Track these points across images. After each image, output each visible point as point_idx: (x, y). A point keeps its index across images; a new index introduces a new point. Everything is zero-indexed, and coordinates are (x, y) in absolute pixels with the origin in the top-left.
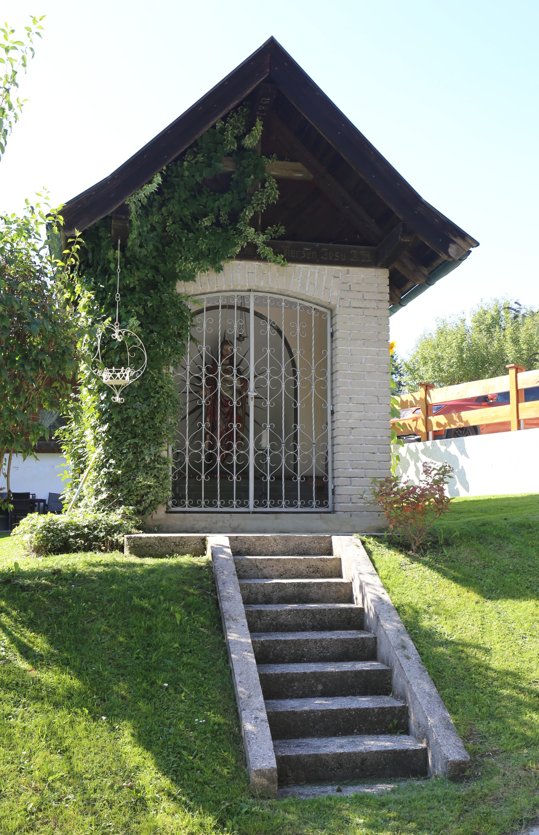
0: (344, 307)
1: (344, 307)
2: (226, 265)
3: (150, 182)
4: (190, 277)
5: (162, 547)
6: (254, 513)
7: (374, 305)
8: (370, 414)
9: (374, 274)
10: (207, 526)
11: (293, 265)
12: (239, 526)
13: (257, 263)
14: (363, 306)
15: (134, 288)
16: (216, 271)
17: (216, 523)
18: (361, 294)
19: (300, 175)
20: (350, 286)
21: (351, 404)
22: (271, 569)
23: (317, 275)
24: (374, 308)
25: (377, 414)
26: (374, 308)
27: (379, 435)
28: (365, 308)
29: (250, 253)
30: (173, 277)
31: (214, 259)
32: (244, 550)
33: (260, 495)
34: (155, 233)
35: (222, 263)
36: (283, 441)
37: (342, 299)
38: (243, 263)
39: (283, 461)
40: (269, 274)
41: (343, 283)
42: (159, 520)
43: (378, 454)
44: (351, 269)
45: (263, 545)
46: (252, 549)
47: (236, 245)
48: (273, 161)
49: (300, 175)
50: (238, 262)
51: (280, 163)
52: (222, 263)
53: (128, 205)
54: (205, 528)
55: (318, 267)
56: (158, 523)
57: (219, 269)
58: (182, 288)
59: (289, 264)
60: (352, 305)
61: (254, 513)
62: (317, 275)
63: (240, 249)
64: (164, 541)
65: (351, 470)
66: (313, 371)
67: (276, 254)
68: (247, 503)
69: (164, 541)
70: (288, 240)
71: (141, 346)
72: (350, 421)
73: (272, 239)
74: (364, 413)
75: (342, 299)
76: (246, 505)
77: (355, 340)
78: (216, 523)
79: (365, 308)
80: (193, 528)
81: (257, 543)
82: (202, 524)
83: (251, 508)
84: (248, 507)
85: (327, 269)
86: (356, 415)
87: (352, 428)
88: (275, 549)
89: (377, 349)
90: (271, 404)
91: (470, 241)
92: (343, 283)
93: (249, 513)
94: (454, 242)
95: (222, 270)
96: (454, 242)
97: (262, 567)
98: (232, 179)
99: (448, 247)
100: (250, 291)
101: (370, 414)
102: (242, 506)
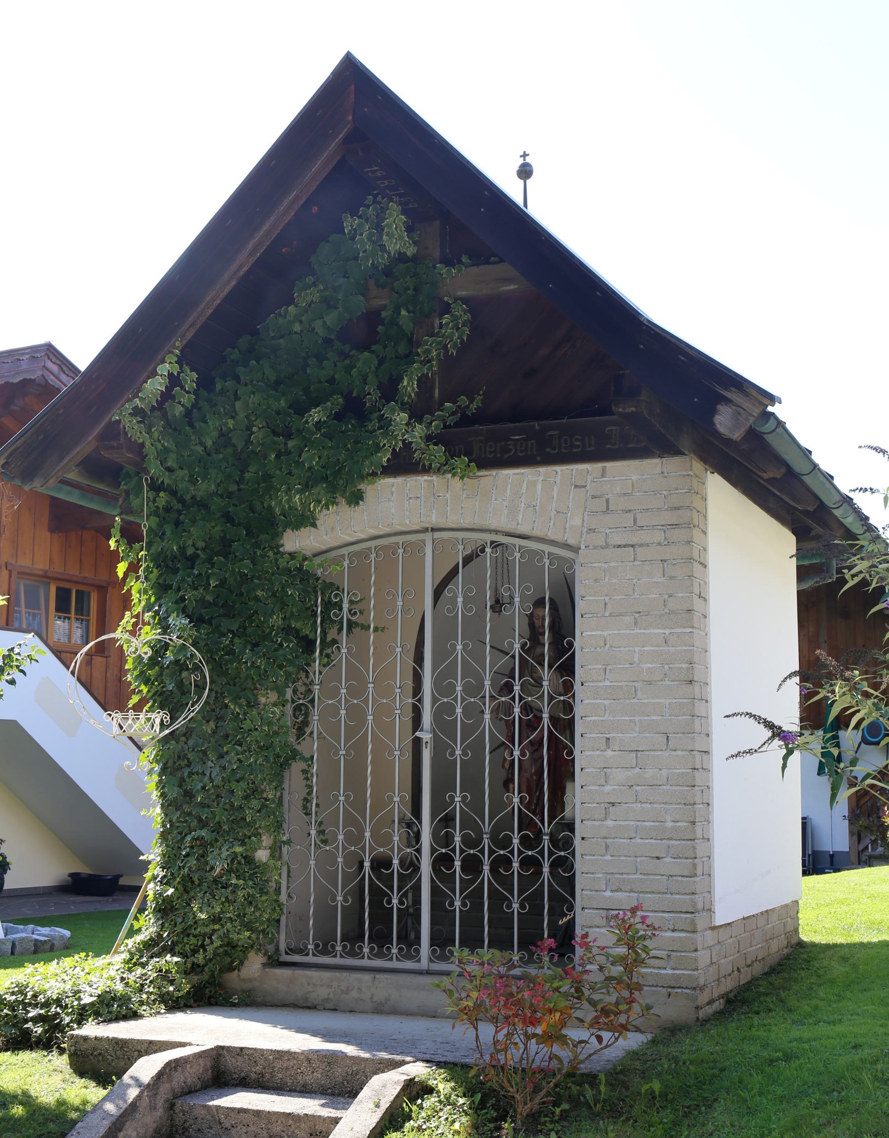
0: (595, 548)
1: (595, 548)
2: (369, 488)
3: (154, 374)
4: (305, 520)
5: (118, 1058)
6: (428, 973)
7: (659, 536)
8: (649, 773)
9: (658, 470)
10: (331, 996)
11: (494, 472)
12: (387, 999)
13: (426, 478)
14: (634, 540)
15: (195, 556)
16: (349, 503)
17: (347, 991)
18: (630, 516)
19: (512, 287)
20: (608, 501)
21: (609, 753)
22: (244, 1129)
23: (539, 486)
24: (659, 544)
25: (664, 772)
26: (659, 544)
27: (668, 818)
28: (641, 545)
29: (404, 464)
30: (269, 527)
31: (342, 483)
32: (253, 1076)
33: (441, 941)
34: (230, 450)
35: (362, 486)
36: (487, 828)
37: (591, 530)
38: (399, 480)
39: (486, 868)
40: (448, 496)
41: (593, 497)
42: (250, 980)
43: (668, 860)
44: (609, 465)
45: (287, 1069)
46: (267, 1076)
47: (378, 448)
48: (459, 271)
49: (512, 287)
50: (389, 480)
51: (474, 270)
52: (362, 486)
53: (119, 422)
54: (327, 1000)
55: (543, 470)
56: (248, 986)
57: (356, 498)
58: (294, 541)
59: (483, 473)
60: (612, 542)
61: (428, 973)
62: (539, 486)
63: (389, 456)
64: (122, 1048)
65: (608, 894)
66: (370, 718)
67: (452, 453)
68: (418, 951)
69: (122, 1048)
70: (480, 424)
71: (200, 661)
72: (607, 788)
73: (445, 427)
74: (637, 770)
75: (591, 530)
76: (415, 956)
77: (620, 615)
78: (347, 991)
79: (641, 545)
80: (306, 999)
81: (278, 1065)
82: (322, 993)
83: (424, 963)
84: (419, 961)
85: (561, 471)
86: (620, 776)
87: (613, 804)
88: (309, 1079)
89: (667, 631)
90: (464, 753)
91: (754, 393)
92: (593, 497)
93: (420, 973)
94: (728, 401)
95: (362, 499)
96: (728, 401)
97: (228, 1125)
98: (382, 322)
99: (713, 412)
100: (426, 530)
101: (649, 773)
102: (408, 957)
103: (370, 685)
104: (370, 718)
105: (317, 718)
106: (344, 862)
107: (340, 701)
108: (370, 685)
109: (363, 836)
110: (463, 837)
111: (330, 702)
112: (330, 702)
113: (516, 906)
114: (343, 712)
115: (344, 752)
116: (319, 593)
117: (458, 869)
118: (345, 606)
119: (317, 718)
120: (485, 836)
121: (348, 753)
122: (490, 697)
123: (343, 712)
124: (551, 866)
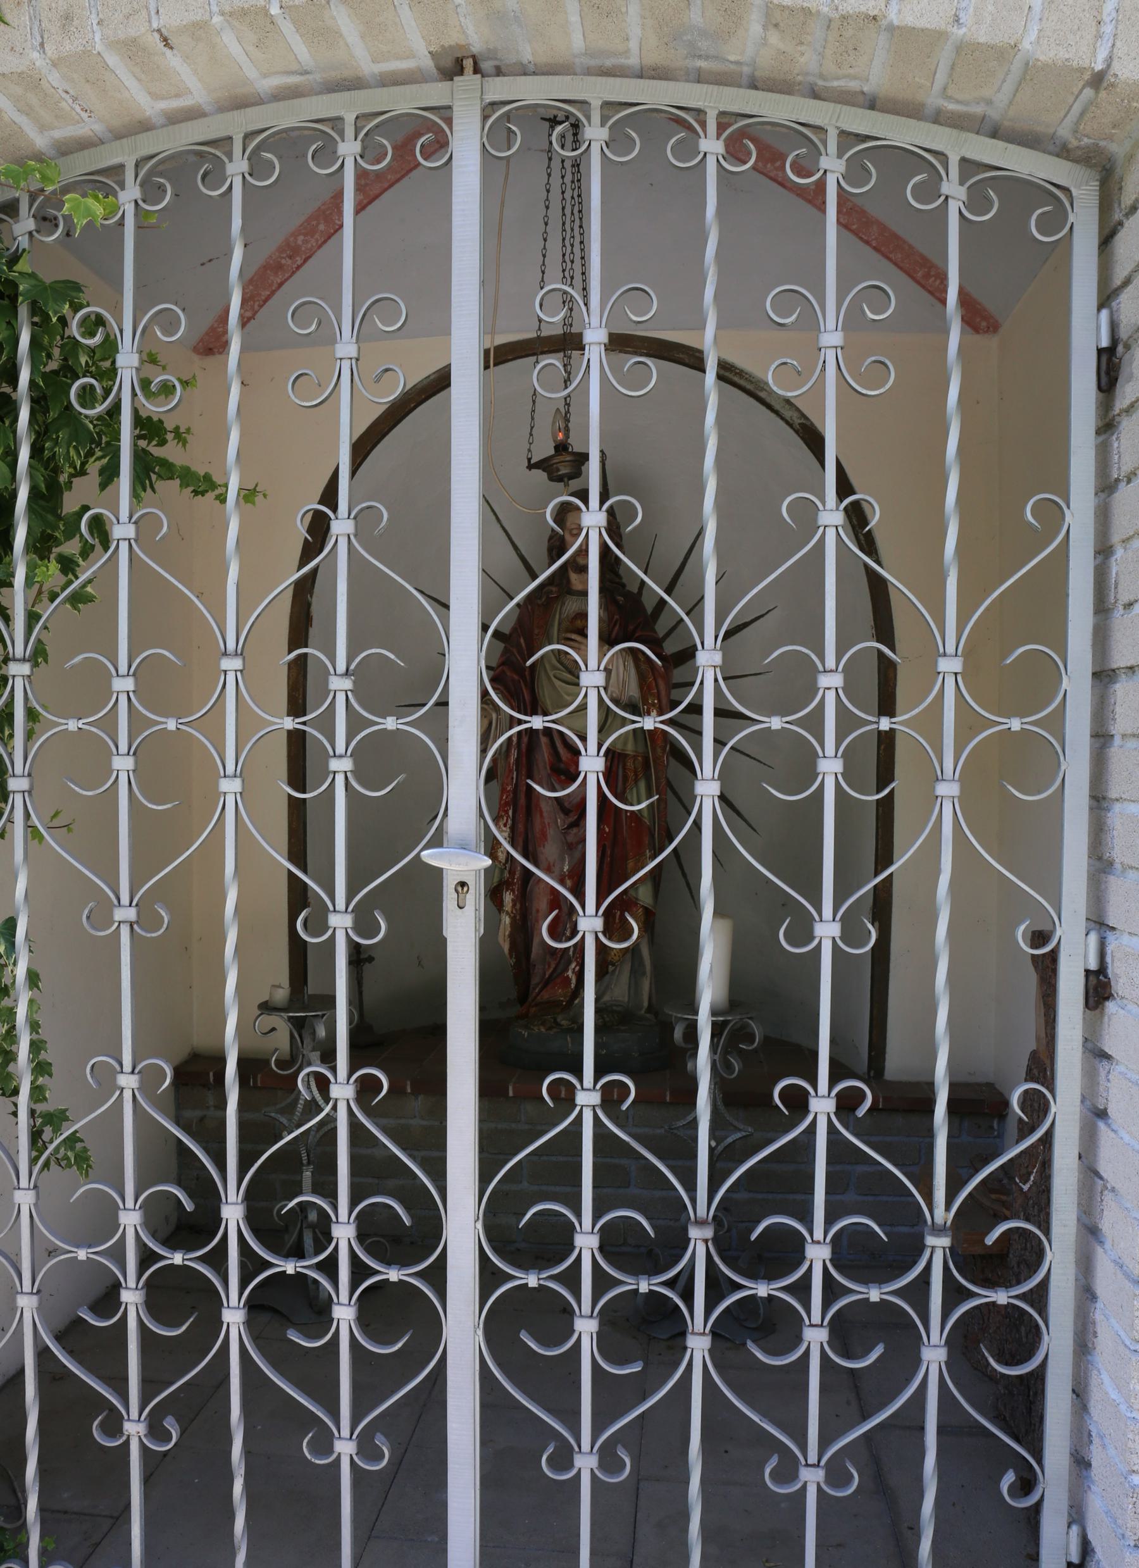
66: (230, 786)
103: (227, 664)
104: (230, 786)
105: (942, 789)
106: (603, 1340)
107: (109, 724)
108: (14, 669)
109: (215, 1220)
110: (148, 1209)
111: (73, 725)
112: (73, 725)
113: (345, 1448)
114: (123, 764)
115: (131, 914)
116: (23, 311)
117: (587, 1348)
118: (127, 360)
119: (942, 789)
120: (694, 1233)
121: (146, 917)
122: (719, 713)
123: (123, 764)
124: (716, 1334)
